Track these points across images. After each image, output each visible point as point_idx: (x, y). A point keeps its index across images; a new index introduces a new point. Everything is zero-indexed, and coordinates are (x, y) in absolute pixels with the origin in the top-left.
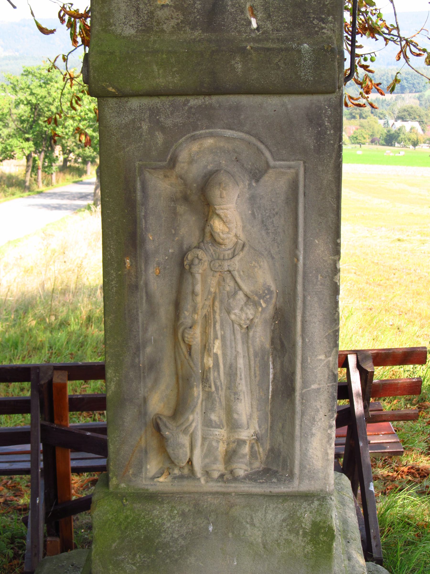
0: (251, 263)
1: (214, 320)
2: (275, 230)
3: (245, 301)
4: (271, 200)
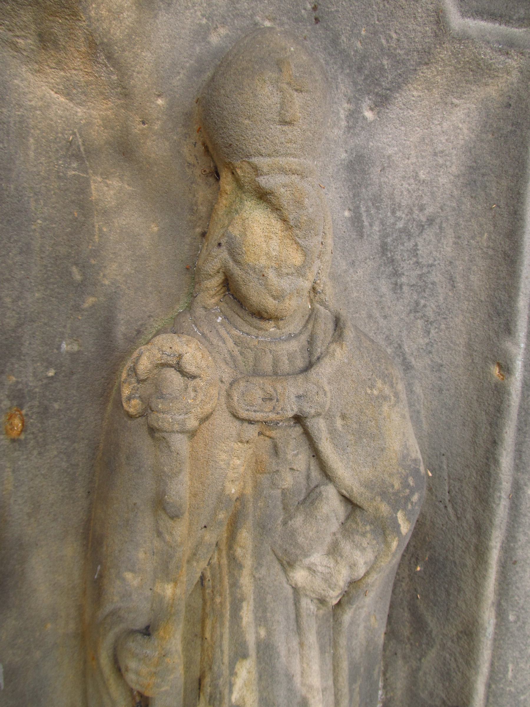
0: (372, 387)
1: (232, 594)
2: (420, 277)
3: (342, 518)
4: (416, 177)
